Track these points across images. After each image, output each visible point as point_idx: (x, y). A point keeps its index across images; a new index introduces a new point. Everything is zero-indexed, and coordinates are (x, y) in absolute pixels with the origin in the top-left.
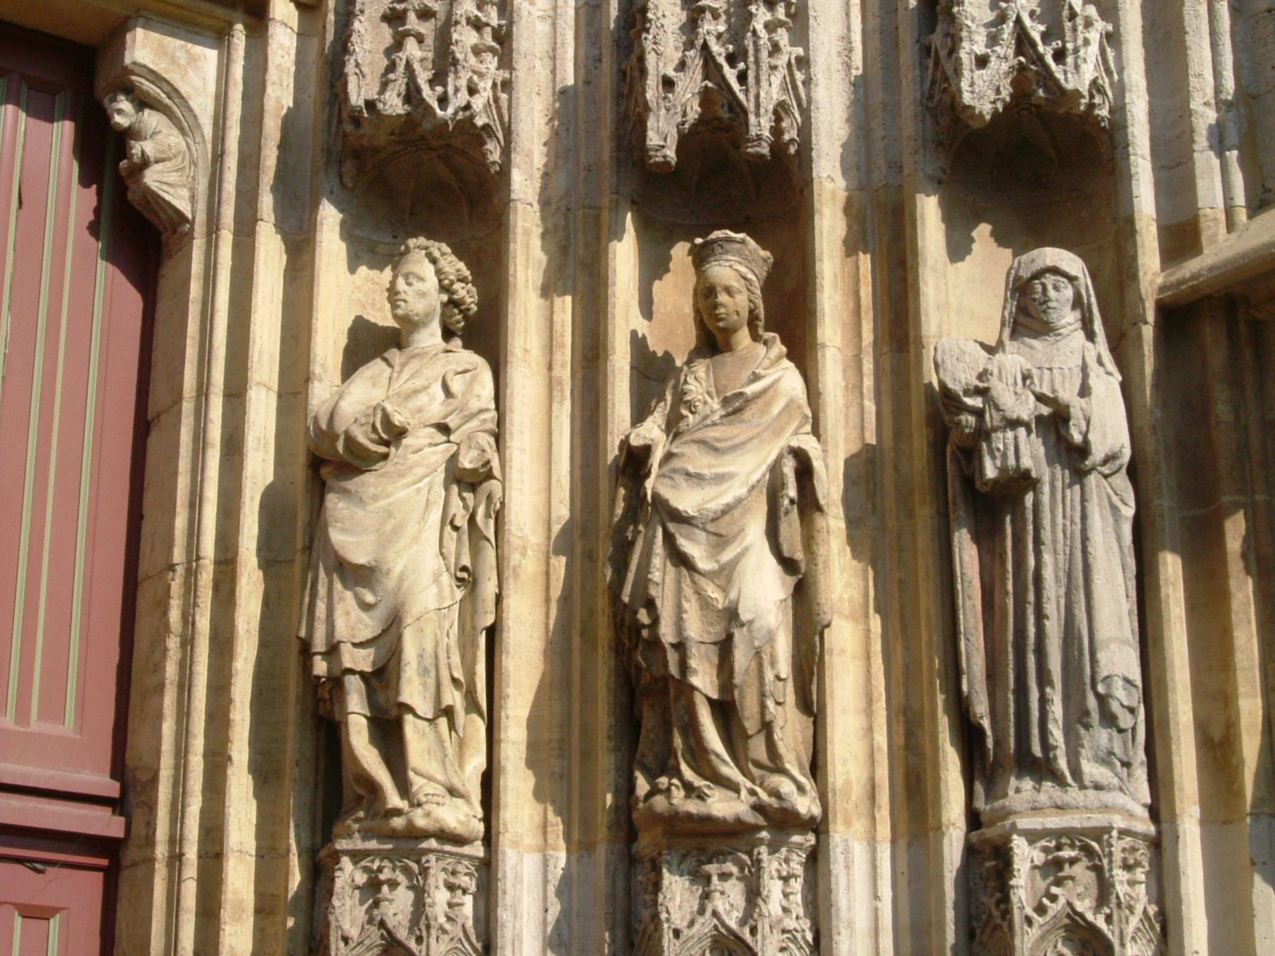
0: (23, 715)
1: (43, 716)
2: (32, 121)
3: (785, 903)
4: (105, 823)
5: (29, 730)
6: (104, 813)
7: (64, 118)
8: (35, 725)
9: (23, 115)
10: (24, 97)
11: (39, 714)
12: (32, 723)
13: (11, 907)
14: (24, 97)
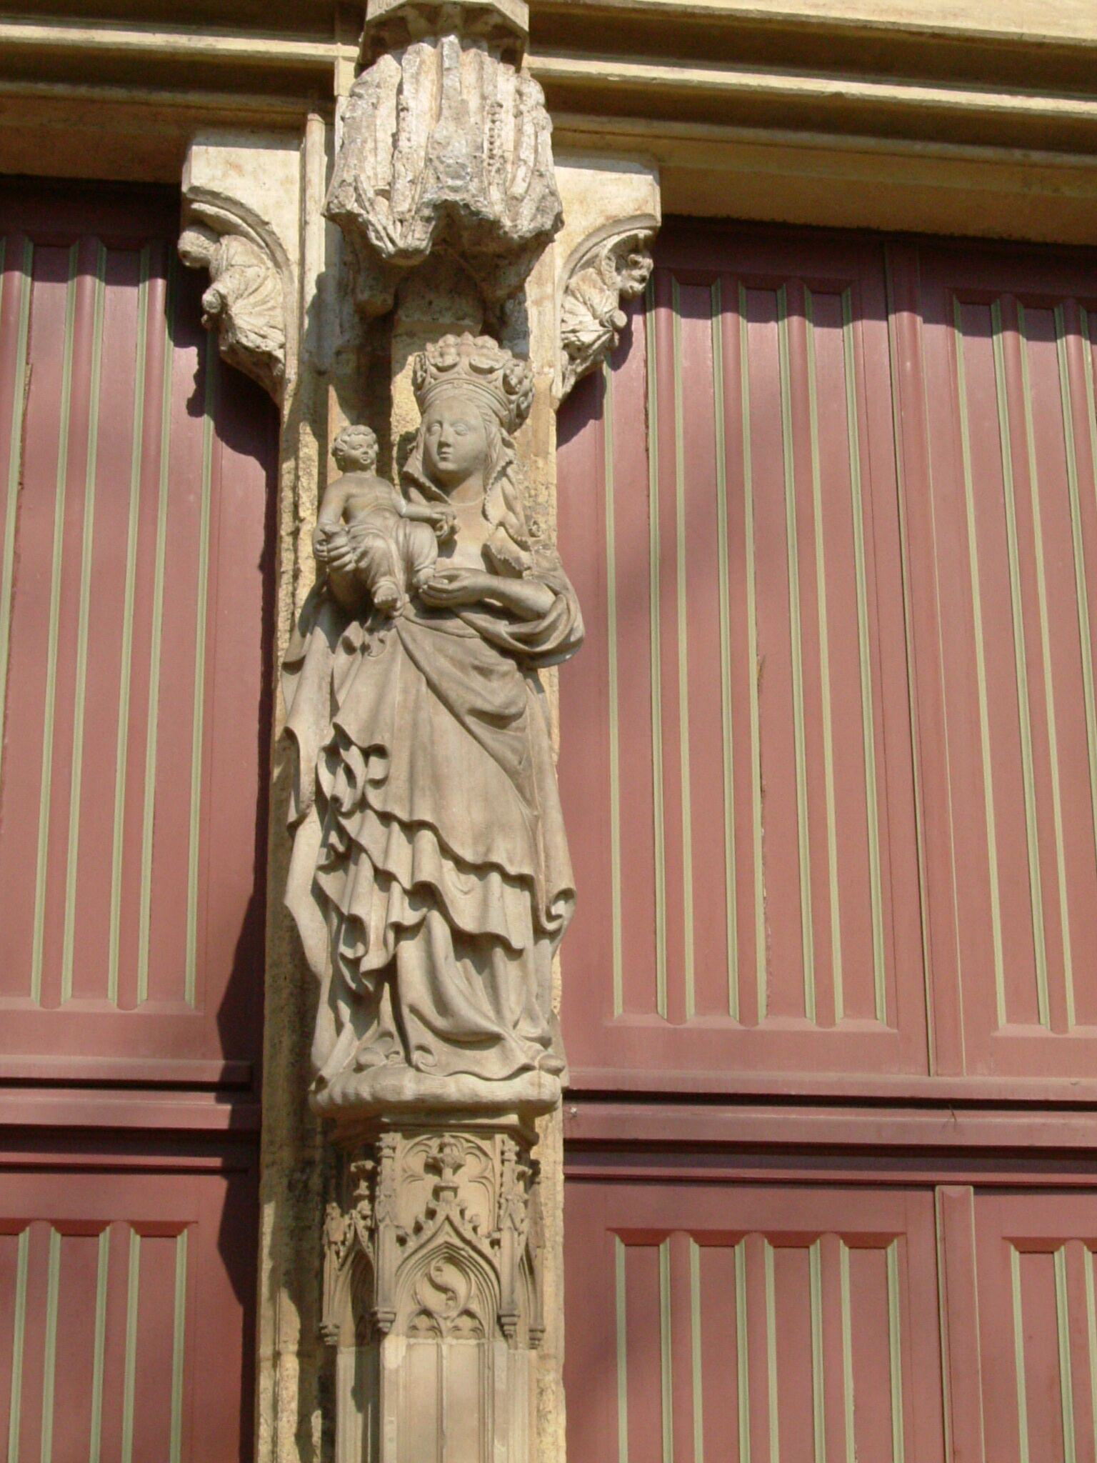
0: (1058, 1019)
1: (702, 1008)
2: (969, 339)
3: (433, 1204)
4: (211, 1113)
5: (1067, 1036)
6: (206, 1101)
7: (1067, 333)
8: (843, 1022)
9: (1023, 340)
10: (1021, 322)
11: (1077, 1017)
12: (838, 1020)
13: (1081, 1244)
14: (1084, 326)
